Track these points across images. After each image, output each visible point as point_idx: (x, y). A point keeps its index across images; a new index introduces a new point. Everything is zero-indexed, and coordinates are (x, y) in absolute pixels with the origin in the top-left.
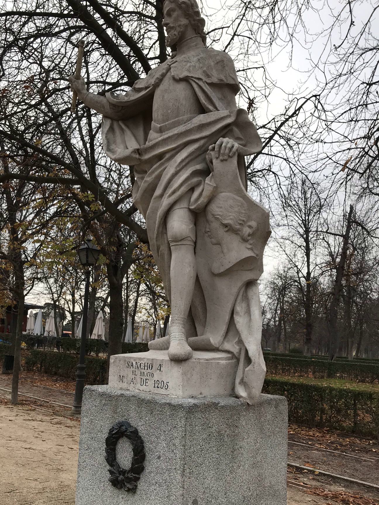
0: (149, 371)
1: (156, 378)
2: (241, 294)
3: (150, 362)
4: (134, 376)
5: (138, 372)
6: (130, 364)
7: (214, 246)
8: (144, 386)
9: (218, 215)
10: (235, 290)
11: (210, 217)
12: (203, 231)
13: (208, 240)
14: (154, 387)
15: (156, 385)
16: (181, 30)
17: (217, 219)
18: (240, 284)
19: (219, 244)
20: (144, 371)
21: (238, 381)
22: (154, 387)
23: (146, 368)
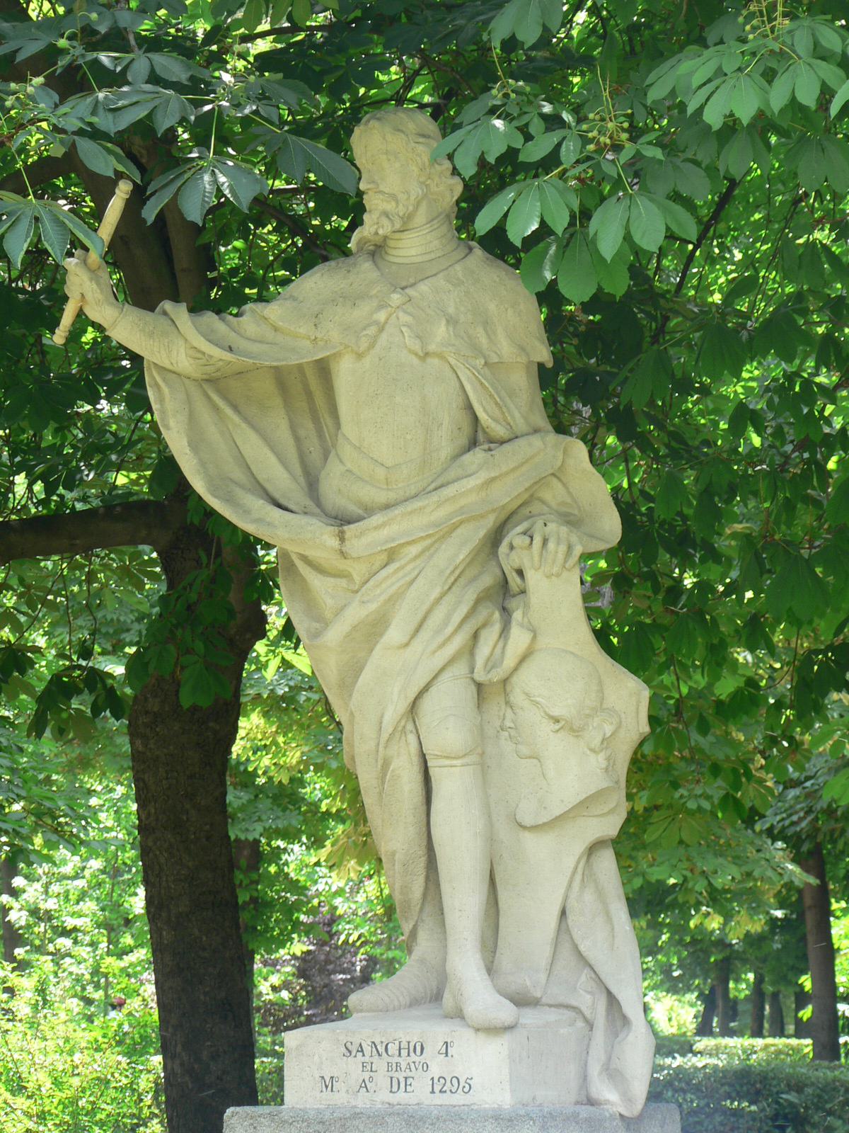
0: (413, 1057)
1: (435, 1071)
2: (580, 870)
3: (416, 1039)
4: (366, 1075)
5: (380, 1064)
6: (354, 1049)
7: (523, 761)
8: (401, 1094)
9: (539, 696)
10: (570, 862)
11: (517, 697)
12: (498, 724)
13: (507, 747)
14: (433, 1092)
15: (437, 1089)
16: (763, 921)
17: (536, 703)
18: (580, 847)
19: (535, 757)
20: (399, 1060)
21: (595, 1069)
22: (433, 1092)
23: (404, 1053)
